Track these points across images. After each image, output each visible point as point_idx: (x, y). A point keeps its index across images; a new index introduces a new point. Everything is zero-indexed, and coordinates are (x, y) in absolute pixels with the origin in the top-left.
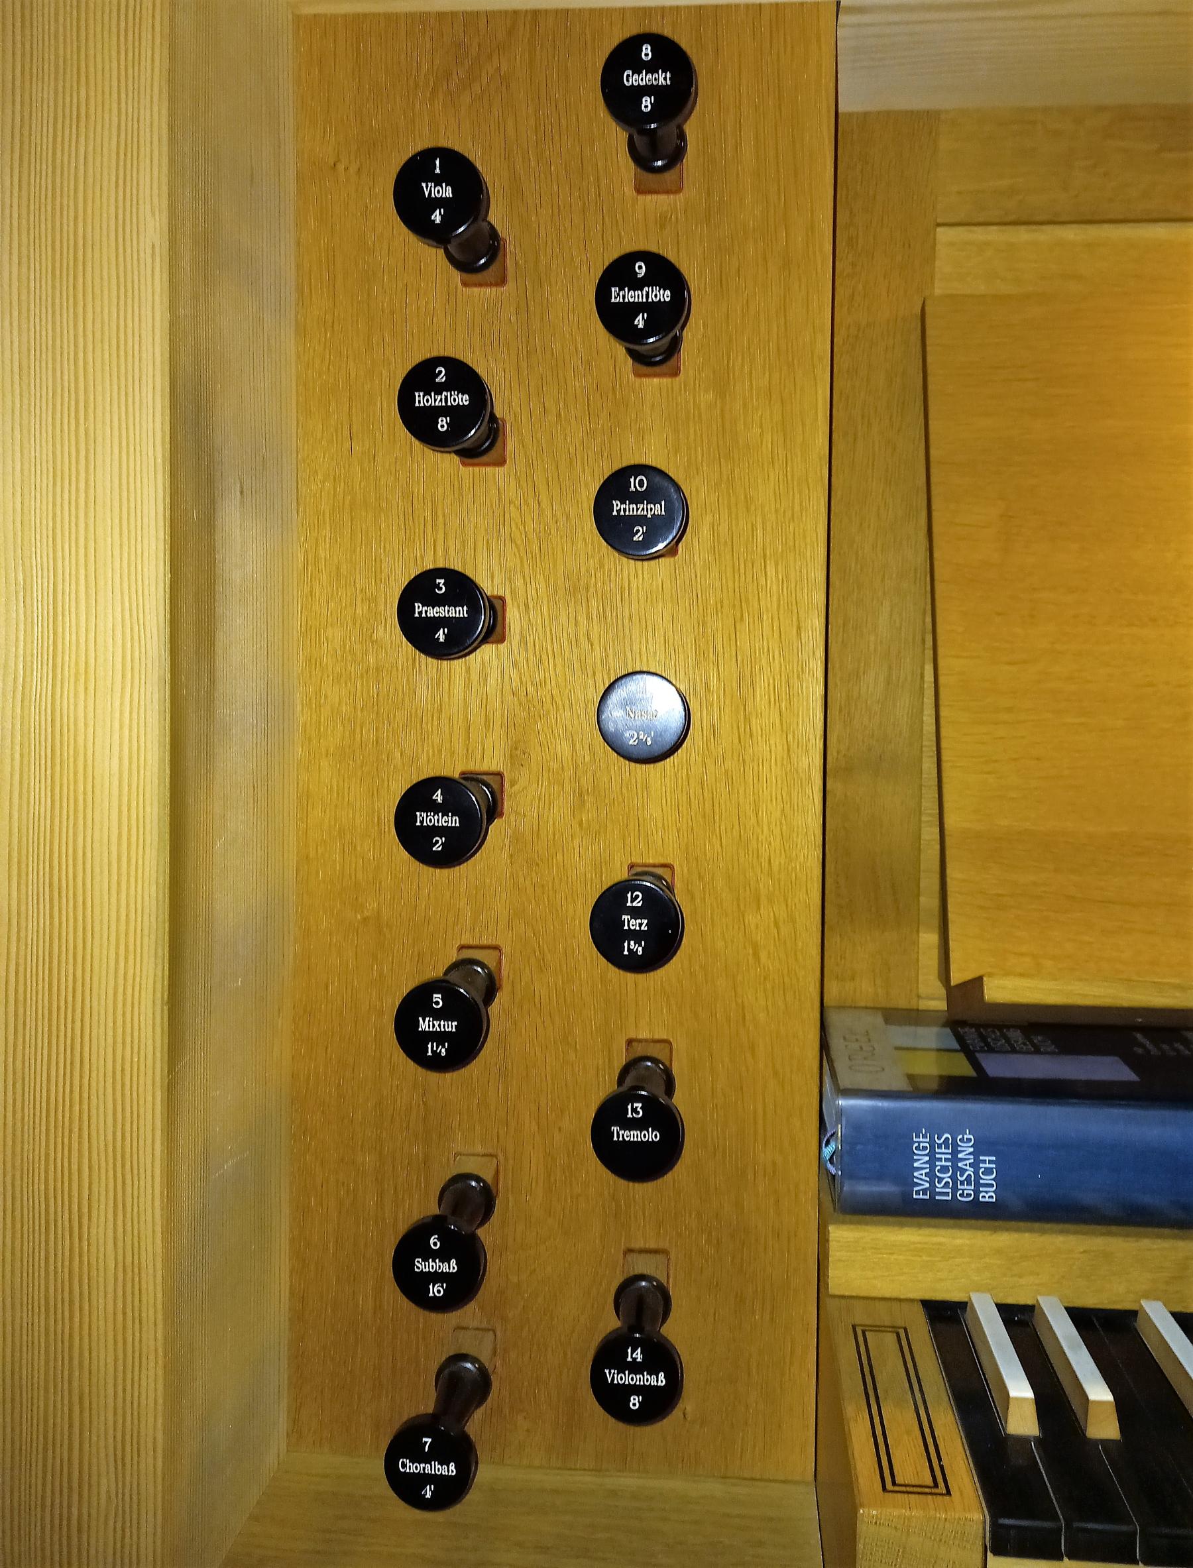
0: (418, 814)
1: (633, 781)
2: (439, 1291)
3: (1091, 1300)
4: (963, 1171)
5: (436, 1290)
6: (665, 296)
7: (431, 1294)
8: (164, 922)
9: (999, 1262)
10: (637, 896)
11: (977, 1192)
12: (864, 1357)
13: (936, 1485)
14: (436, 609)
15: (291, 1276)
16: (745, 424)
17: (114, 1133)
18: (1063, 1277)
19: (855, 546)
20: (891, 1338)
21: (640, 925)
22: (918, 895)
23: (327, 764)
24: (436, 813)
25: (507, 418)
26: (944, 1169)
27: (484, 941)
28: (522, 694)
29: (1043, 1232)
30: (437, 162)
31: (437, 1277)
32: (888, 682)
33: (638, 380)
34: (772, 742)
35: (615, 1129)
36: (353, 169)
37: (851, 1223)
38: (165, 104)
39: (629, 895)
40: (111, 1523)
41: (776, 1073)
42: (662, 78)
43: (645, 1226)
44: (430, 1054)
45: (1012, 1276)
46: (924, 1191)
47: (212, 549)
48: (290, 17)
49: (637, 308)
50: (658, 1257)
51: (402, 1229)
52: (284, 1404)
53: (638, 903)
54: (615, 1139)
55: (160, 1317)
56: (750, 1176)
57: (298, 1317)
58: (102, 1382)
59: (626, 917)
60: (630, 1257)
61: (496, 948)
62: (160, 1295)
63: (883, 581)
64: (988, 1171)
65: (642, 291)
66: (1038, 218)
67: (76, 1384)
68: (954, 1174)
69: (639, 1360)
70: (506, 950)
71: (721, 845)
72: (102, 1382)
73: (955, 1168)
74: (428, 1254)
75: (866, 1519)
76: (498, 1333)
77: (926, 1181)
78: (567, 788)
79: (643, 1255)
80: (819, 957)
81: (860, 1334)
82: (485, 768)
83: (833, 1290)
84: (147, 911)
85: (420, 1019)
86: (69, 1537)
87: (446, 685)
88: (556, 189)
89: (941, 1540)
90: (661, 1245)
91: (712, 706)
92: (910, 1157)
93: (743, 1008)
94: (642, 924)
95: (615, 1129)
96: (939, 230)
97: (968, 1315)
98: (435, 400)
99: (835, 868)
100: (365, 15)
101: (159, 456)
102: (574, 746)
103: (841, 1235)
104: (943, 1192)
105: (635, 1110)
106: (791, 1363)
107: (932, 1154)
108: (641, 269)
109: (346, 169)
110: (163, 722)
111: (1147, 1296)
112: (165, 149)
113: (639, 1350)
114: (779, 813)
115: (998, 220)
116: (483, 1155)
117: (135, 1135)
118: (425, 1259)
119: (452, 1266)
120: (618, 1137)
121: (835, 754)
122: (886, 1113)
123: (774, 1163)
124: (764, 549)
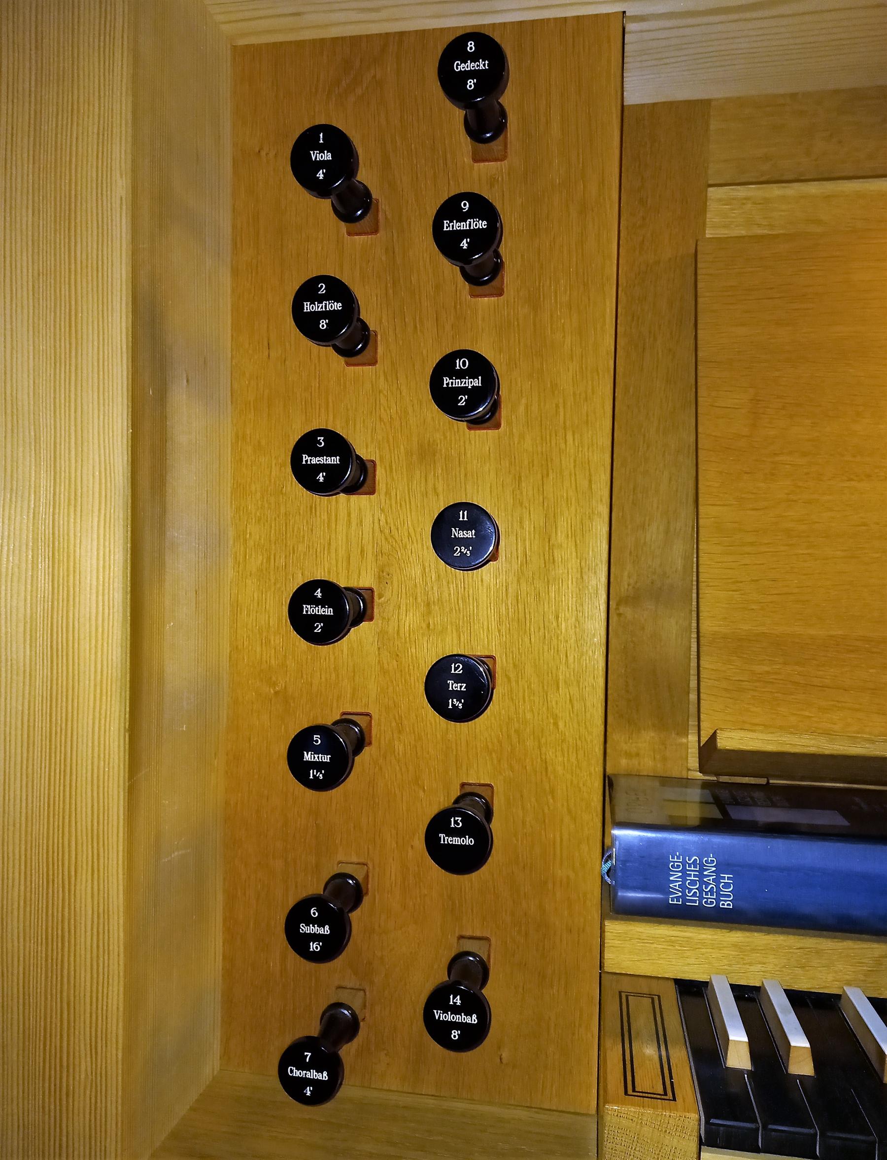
0: (304, 606)
1: (467, 595)
2: (317, 948)
3: (803, 985)
4: (707, 884)
5: (314, 947)
6: (482, 224)
7: (311, 950)
8: (126, 674)
9: (733, 953)
10: (459, 666)
11: (718, 900)
12: (625, 1013)
13: (666, 1094)
14: (318, 459)
15: (223, 946)
16: (551, 330)
17: (92, 821)
18: (784, 967)
19: (643, 430)
20: (647, 1002)
21: (461, 687)
22: (689, 693)
23: (250, 581)
24: (317, 606)
25: (378, 330)
26: (693, 883)
27: (359, 710)
28: (387, 531)
29: (769, 933)
30: (321, 135)
31: (315, 937)
32: (667, 532)
33: (473, 300)
34: (570, 566)
35: (441, 835)
36: (272, 154)
37: (622, 920)
38: (130, 99)
39: (453, 666)
40: (88, 1092)
41: (569, 811)
42: (482, 65)
43: (473, 920)
44: (311, 777)
45: (744, 964)
46: (678, 898)
47: (163, 418)
48: (229, 46)
49: (463, 234)
50: (482, 942)
51: (291, 903)
52: (218, 1034)
53: (459, 671)
54: (442, 842)
55: (122, 950)
56: (550, 886)
57: (229, 973)
58: (82, 995)
59: (450, 682)
60: (462, 941)
61: (368, 714)
62: (122, 934)
63: (664, 455)
64: (727, 885)
65: (466, 222)
66: (785, 178)
67: (65, 994)
68: (701, 886)
69: (458, 1004)
70: (375, 716)
71: (531, 643)
72: (82, 995)
73: (702, 882)
74: (310, 921)
75: (609, 1112)
76: (367, 993)
77: (679, 891)
78: (419, 600)
79: (471, 941)
80: (603, 727)
81: (623, 998)
82: (361, 585)
83: (606, 969)
84: (115, 665)
85: (305, 753)
86: (60, 1099)
87: (334, 526)
88: (415, 162)
89: (666, 1131)
90: (485, 935)
91: (525, 540)
92: (667, 872)
93: (546, 762)
94: (462, 687)
95: (441, 835)
96: (710, 189)
97: (709, 991)
98: (318, 307)
99: (625, 671)
100: (281, 43)
101: (124, 347)
102: (424, 569)
103: (614, 928)
104: (693, 897)
105: (456, 822)
106: (580, 1026)
107: (684, 871)
108: (465, 206)
109: (267, 154)
110: (126, 534)
111: (849, 983)
112: (130, 130)
113: (458, 997)
114: (574, 619)
115: (754, 180)
116: (357, 864)
117: (106, 822)
118: (307, 925)
119: (326, 930)
120: (444, 841)
121: (626, 587)
122: (649, 840)
123: (568, 877)
124: (564, 423)
